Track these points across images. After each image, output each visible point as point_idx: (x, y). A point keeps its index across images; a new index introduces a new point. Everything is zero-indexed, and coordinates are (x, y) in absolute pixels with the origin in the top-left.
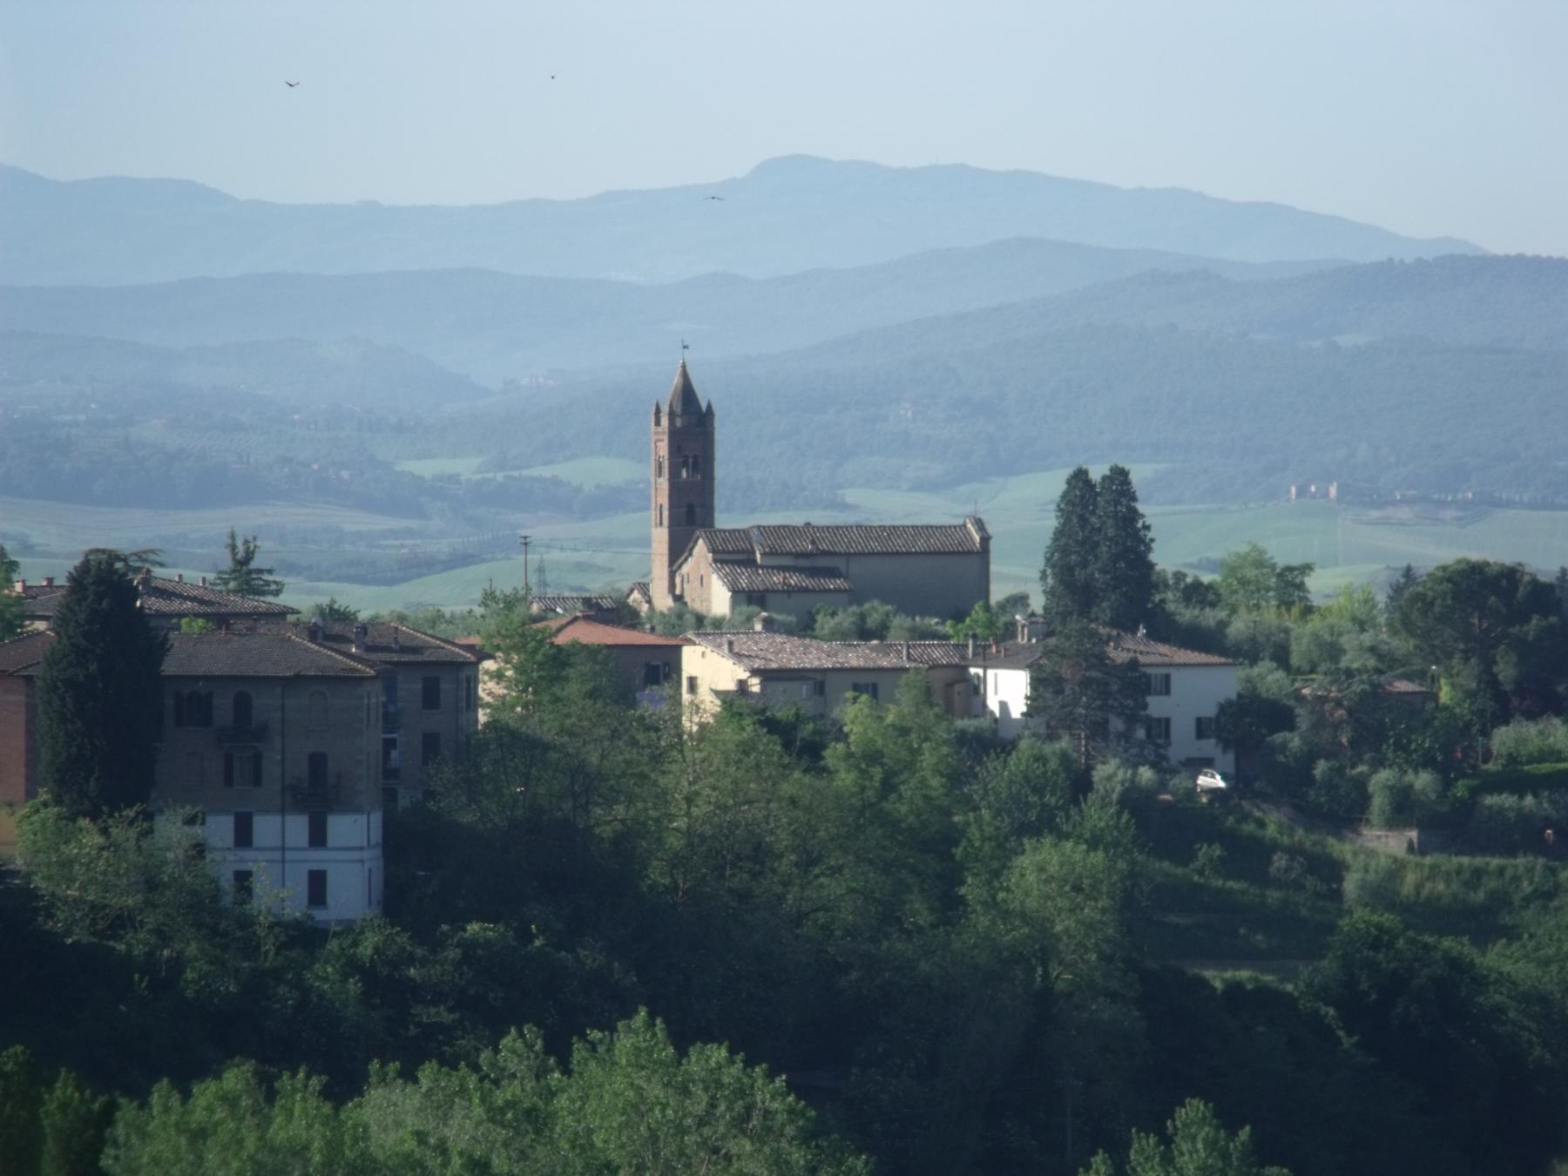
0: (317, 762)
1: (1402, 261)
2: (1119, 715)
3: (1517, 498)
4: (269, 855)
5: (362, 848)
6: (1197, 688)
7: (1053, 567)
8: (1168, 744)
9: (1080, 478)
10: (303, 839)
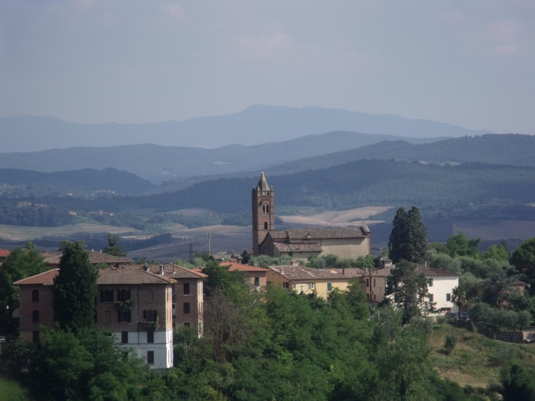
1: (470, 137)
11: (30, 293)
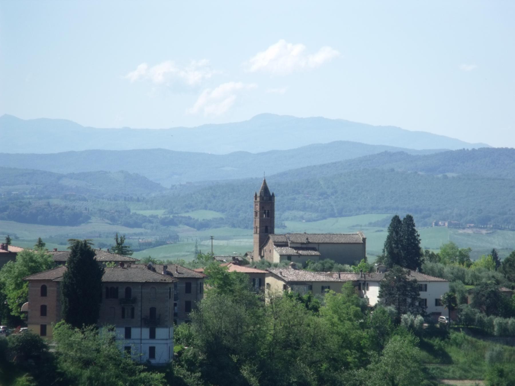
0: (153, 310)
1: (468, 150)
2: (411, 297)
3: (507, 227)
4: (136, 341)
5: (167, 339)
6: (436, 290)
7: (387, 248)
8: (426, 307)
9: (396, 219)
10: (122, 336)
11: (38, 289)
